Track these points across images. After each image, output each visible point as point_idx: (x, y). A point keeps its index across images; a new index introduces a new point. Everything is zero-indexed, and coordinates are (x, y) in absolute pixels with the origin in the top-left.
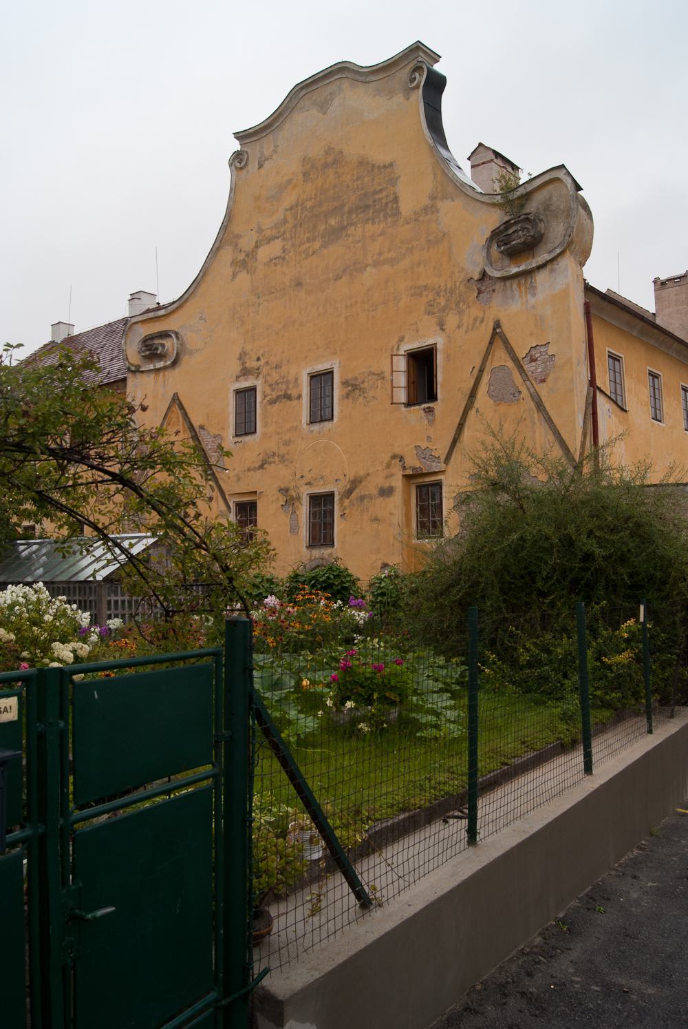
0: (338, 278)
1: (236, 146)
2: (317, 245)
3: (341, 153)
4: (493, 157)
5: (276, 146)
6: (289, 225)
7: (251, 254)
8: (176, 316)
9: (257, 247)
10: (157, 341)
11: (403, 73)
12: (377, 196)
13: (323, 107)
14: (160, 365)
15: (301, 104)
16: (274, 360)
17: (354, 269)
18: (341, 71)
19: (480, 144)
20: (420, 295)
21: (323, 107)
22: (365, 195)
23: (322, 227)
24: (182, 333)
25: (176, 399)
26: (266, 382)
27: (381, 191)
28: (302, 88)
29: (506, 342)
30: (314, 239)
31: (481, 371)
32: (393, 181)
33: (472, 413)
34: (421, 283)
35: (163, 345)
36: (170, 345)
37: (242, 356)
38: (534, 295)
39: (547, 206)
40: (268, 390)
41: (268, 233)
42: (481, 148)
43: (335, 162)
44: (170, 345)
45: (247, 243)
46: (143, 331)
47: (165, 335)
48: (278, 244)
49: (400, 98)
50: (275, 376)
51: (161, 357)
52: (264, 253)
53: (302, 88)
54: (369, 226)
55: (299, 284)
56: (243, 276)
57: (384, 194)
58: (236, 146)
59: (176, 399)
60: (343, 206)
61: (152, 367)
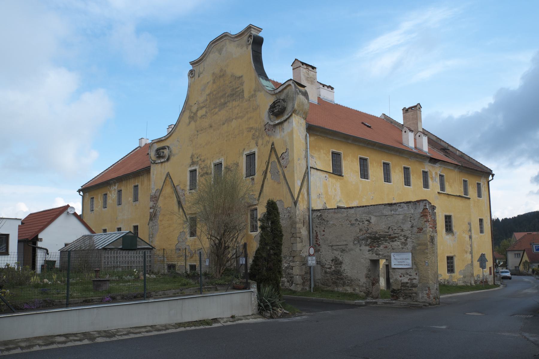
0: (224, 124)
1: (191, 67)
2: (217, 110)
3: (225, 71)
4: (301, 65)
5: (204, 68)
6: (208, 102)
7: (195, 114)
8: (168, 140)
9: (197, 111)
10: (161, 151)
11: (245, 38)
12: (237, 90)
13: (220, 51)
14: (162, 160)
15: (212, 50)
16: (203, 158)
17: (229, 120)
18: (225, 36)
19: (296, 59)
20: (250, 131)
21: (220, 51)
22: (233, 89)
23: (219, 103)
24: (171, 147)
25: (168, 175)
26: (200, 167)
27: (238, 88)
28: (213, 43)
29: (275, 151)
30: (216, 108)
31: (268, 163)
32: (242, 84)
33: (266, 180)
34: (251, 126)
35: (163, 152)
36: (166, 152)
37: (192, 157)
38: (283, 132)
39: (287, 95)
40: (200, 171)
41: (201, 105)
42: (296, 61)
43: (223, 75)
44: (166, 152)
45: (194, 109)
46: (156, 146)
47: (164, 148)
48: (204, 110)
49: (245, 48)
50: (203, 165)
51: (163, 157)
52: (200, 113)
53: (213, 43)
54: (234, 102)
55: (211, 127)
56: (193, 123)
57: (239, 89)
58: (191, 67)
59: (168, 175)
60: (226, 94)
61: (159, 161)
